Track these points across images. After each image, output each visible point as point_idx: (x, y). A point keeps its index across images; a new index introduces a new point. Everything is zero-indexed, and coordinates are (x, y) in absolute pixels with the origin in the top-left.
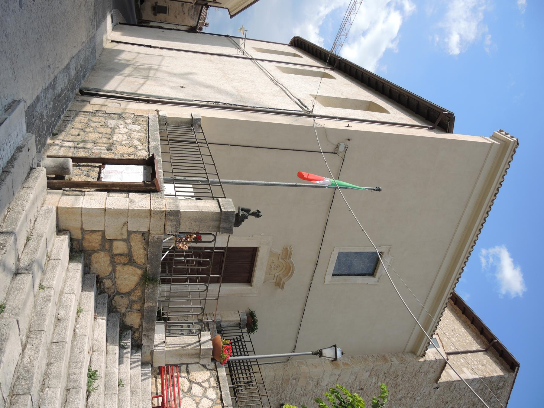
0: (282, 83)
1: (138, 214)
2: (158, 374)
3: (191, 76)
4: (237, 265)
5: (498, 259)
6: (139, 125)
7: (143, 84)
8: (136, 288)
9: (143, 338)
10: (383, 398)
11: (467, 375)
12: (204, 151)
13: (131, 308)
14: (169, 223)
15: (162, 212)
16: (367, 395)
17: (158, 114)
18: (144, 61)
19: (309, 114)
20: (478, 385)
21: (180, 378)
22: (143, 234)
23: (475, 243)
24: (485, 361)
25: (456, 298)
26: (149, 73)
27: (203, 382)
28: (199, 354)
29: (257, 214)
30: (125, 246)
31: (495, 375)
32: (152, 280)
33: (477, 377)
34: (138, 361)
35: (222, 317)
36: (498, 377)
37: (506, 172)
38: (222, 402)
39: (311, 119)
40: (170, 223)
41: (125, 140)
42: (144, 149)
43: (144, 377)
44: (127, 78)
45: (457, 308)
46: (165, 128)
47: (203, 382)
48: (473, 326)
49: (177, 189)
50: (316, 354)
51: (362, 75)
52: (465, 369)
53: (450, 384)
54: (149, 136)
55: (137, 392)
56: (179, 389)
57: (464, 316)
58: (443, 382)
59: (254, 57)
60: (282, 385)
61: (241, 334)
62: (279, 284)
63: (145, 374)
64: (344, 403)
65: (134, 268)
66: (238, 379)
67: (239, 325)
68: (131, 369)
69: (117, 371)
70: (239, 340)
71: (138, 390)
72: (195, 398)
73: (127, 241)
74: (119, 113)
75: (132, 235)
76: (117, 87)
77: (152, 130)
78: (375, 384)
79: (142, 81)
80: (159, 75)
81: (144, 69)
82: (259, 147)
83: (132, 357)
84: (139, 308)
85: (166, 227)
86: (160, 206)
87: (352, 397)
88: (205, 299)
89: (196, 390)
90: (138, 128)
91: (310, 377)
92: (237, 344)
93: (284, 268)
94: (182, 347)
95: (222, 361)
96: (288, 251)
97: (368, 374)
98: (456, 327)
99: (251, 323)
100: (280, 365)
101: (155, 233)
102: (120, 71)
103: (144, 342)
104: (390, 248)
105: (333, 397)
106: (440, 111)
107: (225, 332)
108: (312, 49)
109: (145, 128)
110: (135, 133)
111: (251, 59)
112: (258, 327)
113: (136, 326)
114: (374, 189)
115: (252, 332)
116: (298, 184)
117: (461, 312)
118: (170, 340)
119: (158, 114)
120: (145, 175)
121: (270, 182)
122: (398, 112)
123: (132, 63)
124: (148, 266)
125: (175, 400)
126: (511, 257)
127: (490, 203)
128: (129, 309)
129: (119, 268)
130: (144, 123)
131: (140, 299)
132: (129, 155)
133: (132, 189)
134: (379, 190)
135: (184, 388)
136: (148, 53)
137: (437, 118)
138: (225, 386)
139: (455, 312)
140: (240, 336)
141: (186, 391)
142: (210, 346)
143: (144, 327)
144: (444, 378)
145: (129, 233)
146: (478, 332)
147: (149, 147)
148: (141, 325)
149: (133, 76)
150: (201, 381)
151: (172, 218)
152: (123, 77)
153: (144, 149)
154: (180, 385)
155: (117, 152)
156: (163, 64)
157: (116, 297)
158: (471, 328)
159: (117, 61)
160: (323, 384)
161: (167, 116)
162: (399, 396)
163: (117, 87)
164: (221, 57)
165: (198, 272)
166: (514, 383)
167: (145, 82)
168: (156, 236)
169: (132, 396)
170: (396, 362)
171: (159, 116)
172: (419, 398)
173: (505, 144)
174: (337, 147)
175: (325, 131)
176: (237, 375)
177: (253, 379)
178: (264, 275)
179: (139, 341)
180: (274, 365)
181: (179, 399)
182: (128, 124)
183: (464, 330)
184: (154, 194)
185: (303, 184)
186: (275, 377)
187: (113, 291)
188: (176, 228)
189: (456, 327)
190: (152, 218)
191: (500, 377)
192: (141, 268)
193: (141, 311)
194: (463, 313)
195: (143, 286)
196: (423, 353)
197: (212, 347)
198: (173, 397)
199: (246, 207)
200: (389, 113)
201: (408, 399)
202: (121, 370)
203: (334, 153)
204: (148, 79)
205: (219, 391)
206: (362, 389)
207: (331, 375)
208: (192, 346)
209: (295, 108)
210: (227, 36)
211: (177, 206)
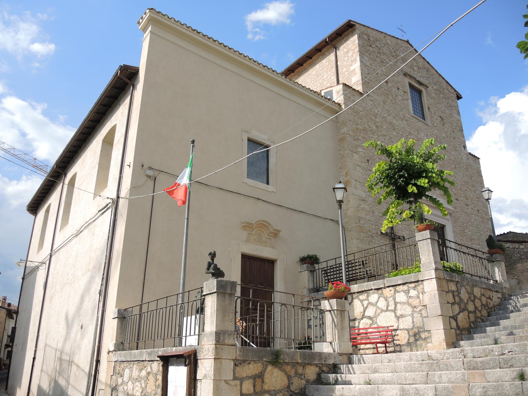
0: (79, 227)
1: (218, 370)
2: (356, 347)
3: (70, 317)
4: (258, 273)
5: (257, 24)
6: (124, 370)
7: (77, 366)
8: (284, 371)
9: (327, 362)
10: (377, 145)
11: (357, 66)
12: (153, 306)
13: (301, 375)
14: (227, 342)
15: (216, 348)
16: (373, 156)
17: (112, 352)
18: (51, 364)
19: (116, 202)
20: (366, 57)
21: (360, 327)
22: (235, 365)
23: (241, 54)
24: (345, 50)
25: (288, 71)
26: (65, 360)
27: (363, 305)
28: (342, 311)
29: (213, 255)
30: (247, 382)
31: (357, 42)
32: (277, 356)
33: (358, 58)
34: (348, 367)
35: (305, 288)
36: (359, 40)
37: (178, 21)
38: (381, 288)
39: (121, 201)
40: (227, 340)
41: (141, 384)
42: (151, 365)
43: (362, 362)
44: (71, 382)
45: (297, 70)
46: (127, 345)
47: (363, 305)
48: (314, 58)
49: (192, 333)
50: (340, 206)
51: (74, 146)
52: (352, 68)
53: (365, 83)
54: (136, 361)
55: (375, 367)
56: (369, 328)
57: (304, 65)
58: (363, 88)
59: (49, 252)
60: (364, 232)
61: (320, 270)
62: (276, 234)
63: (359, 360)
64: (381, 179)
65: (266, 373)
66: (360, 274)
67: (312, 272)
68: (355, 373)
69: (358, 386)
70: (326, 272)
71: (373, 367)
72: (377, 314)
73: (242, 380)
74: (110, 390)
75: (237, 375)
76: (80, 392)
77: (131, 358)
78: (364, 149)
79: (74, 368)
80: (67, 349)
81: (61, 365)
82: (147, 252)
83: (345, 372)
84: (301, 368)
85: (230, 343)
86: (211, 350)
87: (376, 172)
88: (294, 306)
89: (370, 312)
90: (127, 371)
91: (358, 207)
92: (329, 274)
93: (261, 229)
94: (335, 327)
95: (347, 290)
96: (245, 226)
97: (355, 155)
98: (314, 73)
99: (310, 261)
100: (347, 234)
101: (235, 354)
102: (62, 389)
103: (331, 362)
104: (244, 131)
105: (376, 189)
106: (117, 77)
107: (318, 284)
108: (41, 193)
109: (127, 365)
110: (134, 374)
111: (51, 256)
112: (313, 254)
113: (317, 369)
114: (193, 146)
115: (319, 260)
116: (186, 217)
117: (301, 68)
118: (329, 338)
119: (112, 352)
120: (178, 364)
121: (184, 243)
122: (115, 116)
123: (53, 377)
124: (264, 359)
125: (379, 332)
126: (256, 11)
127: (206, 38)
128: (303, 377)
129: (266, 387)
130: (122, 366)
131: (294, 366)
132: (156, 380)
133: (193, 377)
134: (193, 142)
135: (369, 324)
136: (41, 361)
137: (123, 82)
138: (367, 286)
139: (301, 73)
140: (322, 271)
141: (371, 322)
142: (334, 301)
143: (318, 362)
144: (360, 88)
145: (235, 378)
146: (319, 53)
147: (148, 361)
148: (316, 365)
149: (69, 377)
150: (362, 307)
151: (222, 338)
152: (70, 387)
153: (151, 365)
154: (366, 327)
155: (154, 392)
156: (55, 346)
157: (291, 389)
158: (316, 60)
159: (51, 393)
160: (363, 195)
161: (114, 342)
162: (374, 128)
163: (80, 392)
164: (48, 286)
165: (262, 311)
166: (364, 26)
167: (75, 364)
168: (238, 353)
169: (379, 372)
170: (345, 130)
171: (114, 350)
172: (376, 111)
173: (151, 20)
174: (149, 177)
175: (134, 188)
176: (357, 274)
177: (361, 260)
178: (267, 248)
179: (330, 367)
180: (347, 239)
181: (378, 328)
182: (123, 381)
183: (317, 66)
184: (198, 356)
185: (187, 212)
186: (358, 239)
187: (286, 393)
188: (231, 334)
189: (314, 73)
190: (222, 357)
191: (359, 38)
192: (267, 366)
193: (304, 365)
194: (302, 65)
195: (282, 365)
196: (337, 105)
197: (335, 300)
198: (376, 334)
199: (206, 266)
200: (115, 126)
201: (377, 120)
202: (356, 383)
203: (155, 180)
204: (72, 361)
205: (371, 292)
206: (368, 161)
207: (356, 188)
208: (334, 318)
209: (108, 215)
210: (23, 279)
211: (211, 334)
